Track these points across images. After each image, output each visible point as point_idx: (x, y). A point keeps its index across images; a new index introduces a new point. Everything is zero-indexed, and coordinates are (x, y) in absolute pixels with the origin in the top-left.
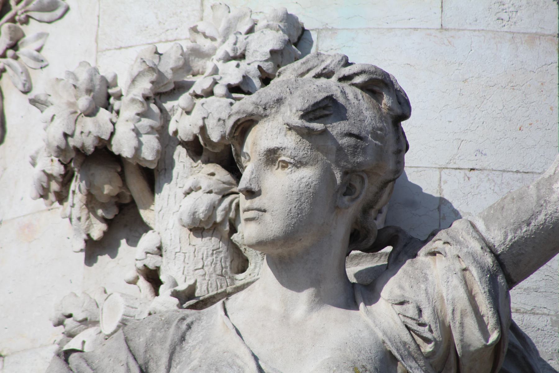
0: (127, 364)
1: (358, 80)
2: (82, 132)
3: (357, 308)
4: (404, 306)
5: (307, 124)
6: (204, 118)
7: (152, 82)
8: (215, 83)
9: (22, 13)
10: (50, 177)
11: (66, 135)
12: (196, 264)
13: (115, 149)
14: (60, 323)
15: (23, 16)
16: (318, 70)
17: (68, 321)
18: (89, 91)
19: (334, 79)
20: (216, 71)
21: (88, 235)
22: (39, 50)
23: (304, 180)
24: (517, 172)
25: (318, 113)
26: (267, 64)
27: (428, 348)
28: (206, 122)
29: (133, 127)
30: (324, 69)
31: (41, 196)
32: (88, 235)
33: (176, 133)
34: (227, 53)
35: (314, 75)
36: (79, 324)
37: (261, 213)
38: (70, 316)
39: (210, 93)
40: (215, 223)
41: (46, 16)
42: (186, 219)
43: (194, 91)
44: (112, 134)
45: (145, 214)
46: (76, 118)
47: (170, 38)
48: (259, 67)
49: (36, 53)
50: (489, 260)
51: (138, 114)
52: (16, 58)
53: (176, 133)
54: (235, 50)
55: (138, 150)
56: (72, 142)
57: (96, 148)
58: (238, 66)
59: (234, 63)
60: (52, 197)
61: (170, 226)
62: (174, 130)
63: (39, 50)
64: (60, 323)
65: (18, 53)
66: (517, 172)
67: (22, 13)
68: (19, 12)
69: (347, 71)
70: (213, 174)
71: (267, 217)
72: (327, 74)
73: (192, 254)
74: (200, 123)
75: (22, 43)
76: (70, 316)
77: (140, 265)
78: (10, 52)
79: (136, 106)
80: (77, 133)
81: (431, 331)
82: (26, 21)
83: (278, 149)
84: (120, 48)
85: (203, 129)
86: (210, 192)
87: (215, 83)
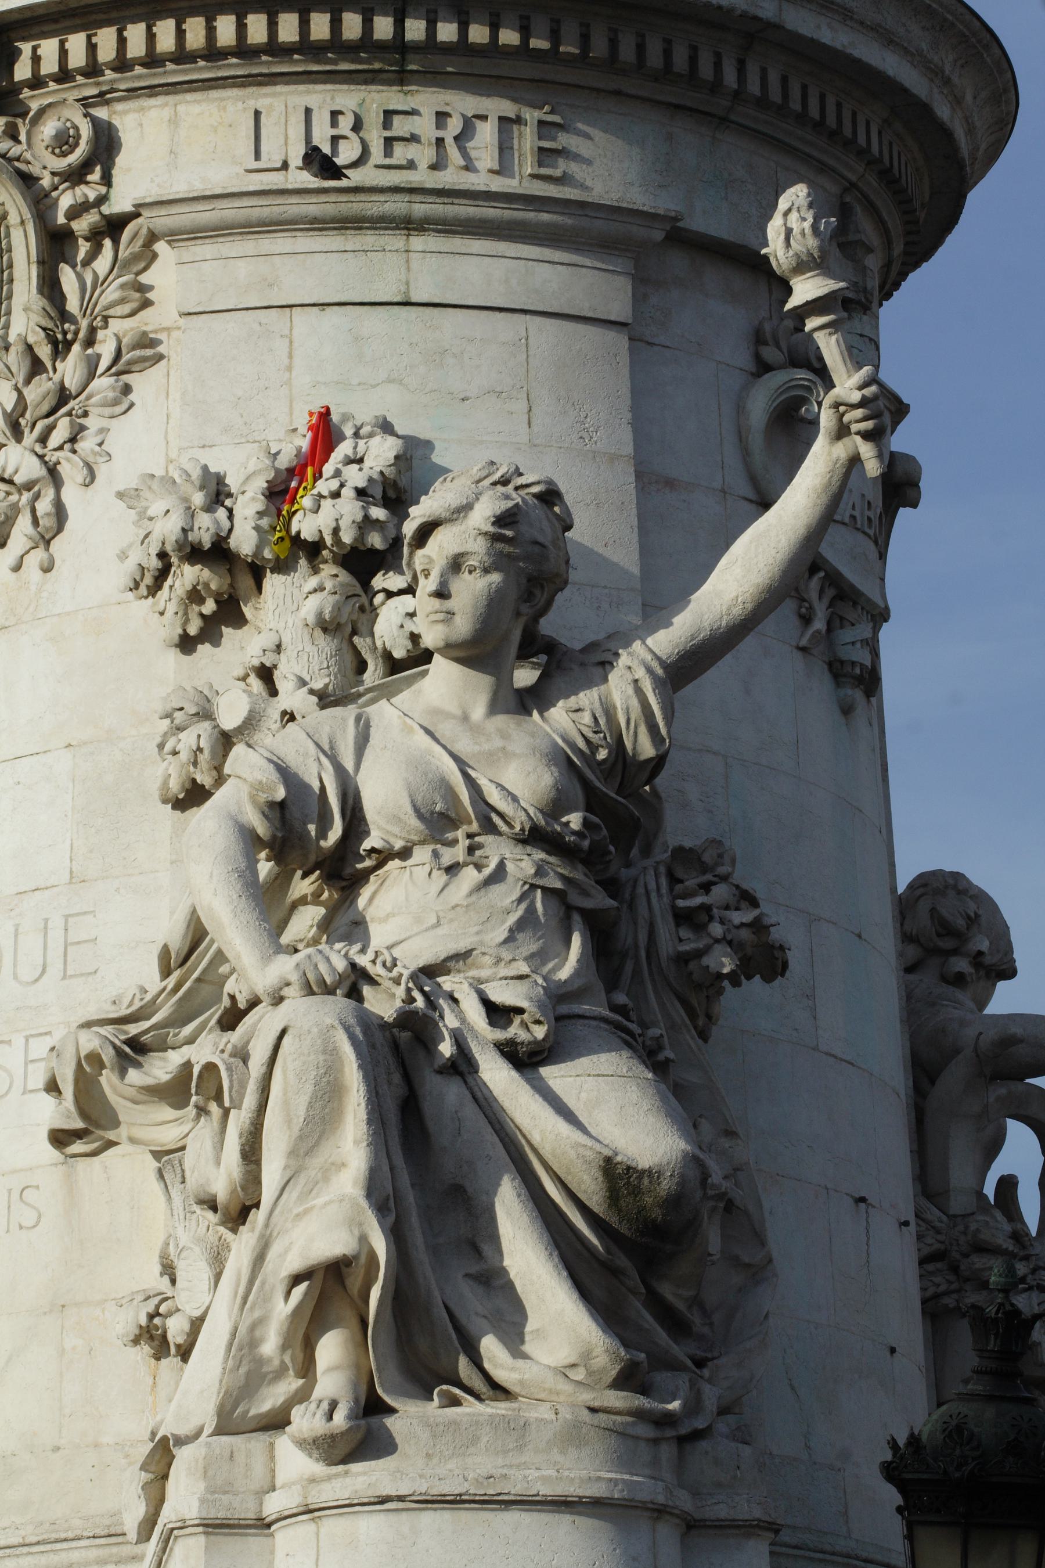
0: (318, 759)
1: (535, 489)
2: (200, 528)
3: (530, 715)
4: (579, 714)
5: (499, 531)
6: (337, 520)
7: (267, 482)
8: (342, 485)
9: (80, 408)
10: (143, 569)
11: (184, 530)
12: (321, 663)
13: (233, 543)
14: (168, 715)
15: (80, 411)
16: (496, 477)
17: (178, 715)
18: (202, 488)
19: (511, 486)
20: (337, 473)
21: (185, 630)
22: (100, 445)
23: (494, 586)
24: (605, 587)
25: (508, 520)
26: (389, 468)
27: (602, 754)
28: (340, 522)
29: (254, 525)
30: (502, 476)
31: (131, 590)
32: (185, 630)
33: (299, 533)
34: (346, 456)
35: (491, 482)
36: (190, 717)
37: (449, 616)
38: (182, 709)
39: (336, 495)
40: (339, 624)
41: (108, 411)
42: (311, 619)
43: (319, 493)
44: (230, 530)
45: (247, 611)
46: (191, 514)
47: (257, 439)
48: (382, 473)
49: (97, 448)
50: (660, 671)
51: (258, 513)
52: (74, 452)
53: (299, 533)
54: (355, 453)
55: (259, 548)
56: (191, 537)
57: (213, 544)
58: (361, 469)
59: (356, 467)
60: (143, 590)
61: (290, 624)
62: (297, 529)
63: (100, 445)
64: (168, 715)
65: (77, 446)
66: (605, 587)
67: (80, 408)
68: (77, 407)
69: (520, 481)
70: (336, 576)
71: (458, 620)
72: (504, 482)
73: (316, 653)
74: (334, 525)
75: (81, 437)
76: (182, 709)
77: (256, 662)
78: (67, 446)
79: (256, 504)
80: (196, 528)
81: (605, 738)
82: (85, 414)
83: (467, 553)
84: (204, 447)
85: (336, 531)
86: (336, 593)
87: (342, 485)
